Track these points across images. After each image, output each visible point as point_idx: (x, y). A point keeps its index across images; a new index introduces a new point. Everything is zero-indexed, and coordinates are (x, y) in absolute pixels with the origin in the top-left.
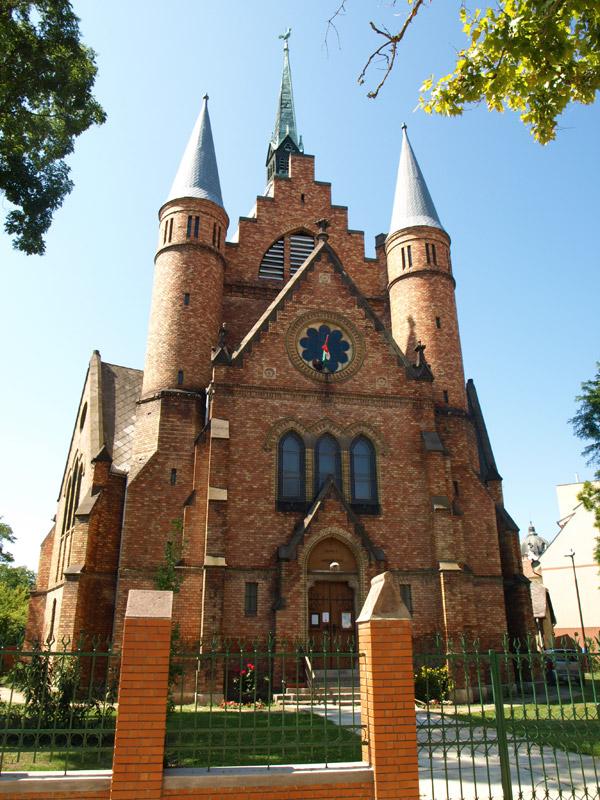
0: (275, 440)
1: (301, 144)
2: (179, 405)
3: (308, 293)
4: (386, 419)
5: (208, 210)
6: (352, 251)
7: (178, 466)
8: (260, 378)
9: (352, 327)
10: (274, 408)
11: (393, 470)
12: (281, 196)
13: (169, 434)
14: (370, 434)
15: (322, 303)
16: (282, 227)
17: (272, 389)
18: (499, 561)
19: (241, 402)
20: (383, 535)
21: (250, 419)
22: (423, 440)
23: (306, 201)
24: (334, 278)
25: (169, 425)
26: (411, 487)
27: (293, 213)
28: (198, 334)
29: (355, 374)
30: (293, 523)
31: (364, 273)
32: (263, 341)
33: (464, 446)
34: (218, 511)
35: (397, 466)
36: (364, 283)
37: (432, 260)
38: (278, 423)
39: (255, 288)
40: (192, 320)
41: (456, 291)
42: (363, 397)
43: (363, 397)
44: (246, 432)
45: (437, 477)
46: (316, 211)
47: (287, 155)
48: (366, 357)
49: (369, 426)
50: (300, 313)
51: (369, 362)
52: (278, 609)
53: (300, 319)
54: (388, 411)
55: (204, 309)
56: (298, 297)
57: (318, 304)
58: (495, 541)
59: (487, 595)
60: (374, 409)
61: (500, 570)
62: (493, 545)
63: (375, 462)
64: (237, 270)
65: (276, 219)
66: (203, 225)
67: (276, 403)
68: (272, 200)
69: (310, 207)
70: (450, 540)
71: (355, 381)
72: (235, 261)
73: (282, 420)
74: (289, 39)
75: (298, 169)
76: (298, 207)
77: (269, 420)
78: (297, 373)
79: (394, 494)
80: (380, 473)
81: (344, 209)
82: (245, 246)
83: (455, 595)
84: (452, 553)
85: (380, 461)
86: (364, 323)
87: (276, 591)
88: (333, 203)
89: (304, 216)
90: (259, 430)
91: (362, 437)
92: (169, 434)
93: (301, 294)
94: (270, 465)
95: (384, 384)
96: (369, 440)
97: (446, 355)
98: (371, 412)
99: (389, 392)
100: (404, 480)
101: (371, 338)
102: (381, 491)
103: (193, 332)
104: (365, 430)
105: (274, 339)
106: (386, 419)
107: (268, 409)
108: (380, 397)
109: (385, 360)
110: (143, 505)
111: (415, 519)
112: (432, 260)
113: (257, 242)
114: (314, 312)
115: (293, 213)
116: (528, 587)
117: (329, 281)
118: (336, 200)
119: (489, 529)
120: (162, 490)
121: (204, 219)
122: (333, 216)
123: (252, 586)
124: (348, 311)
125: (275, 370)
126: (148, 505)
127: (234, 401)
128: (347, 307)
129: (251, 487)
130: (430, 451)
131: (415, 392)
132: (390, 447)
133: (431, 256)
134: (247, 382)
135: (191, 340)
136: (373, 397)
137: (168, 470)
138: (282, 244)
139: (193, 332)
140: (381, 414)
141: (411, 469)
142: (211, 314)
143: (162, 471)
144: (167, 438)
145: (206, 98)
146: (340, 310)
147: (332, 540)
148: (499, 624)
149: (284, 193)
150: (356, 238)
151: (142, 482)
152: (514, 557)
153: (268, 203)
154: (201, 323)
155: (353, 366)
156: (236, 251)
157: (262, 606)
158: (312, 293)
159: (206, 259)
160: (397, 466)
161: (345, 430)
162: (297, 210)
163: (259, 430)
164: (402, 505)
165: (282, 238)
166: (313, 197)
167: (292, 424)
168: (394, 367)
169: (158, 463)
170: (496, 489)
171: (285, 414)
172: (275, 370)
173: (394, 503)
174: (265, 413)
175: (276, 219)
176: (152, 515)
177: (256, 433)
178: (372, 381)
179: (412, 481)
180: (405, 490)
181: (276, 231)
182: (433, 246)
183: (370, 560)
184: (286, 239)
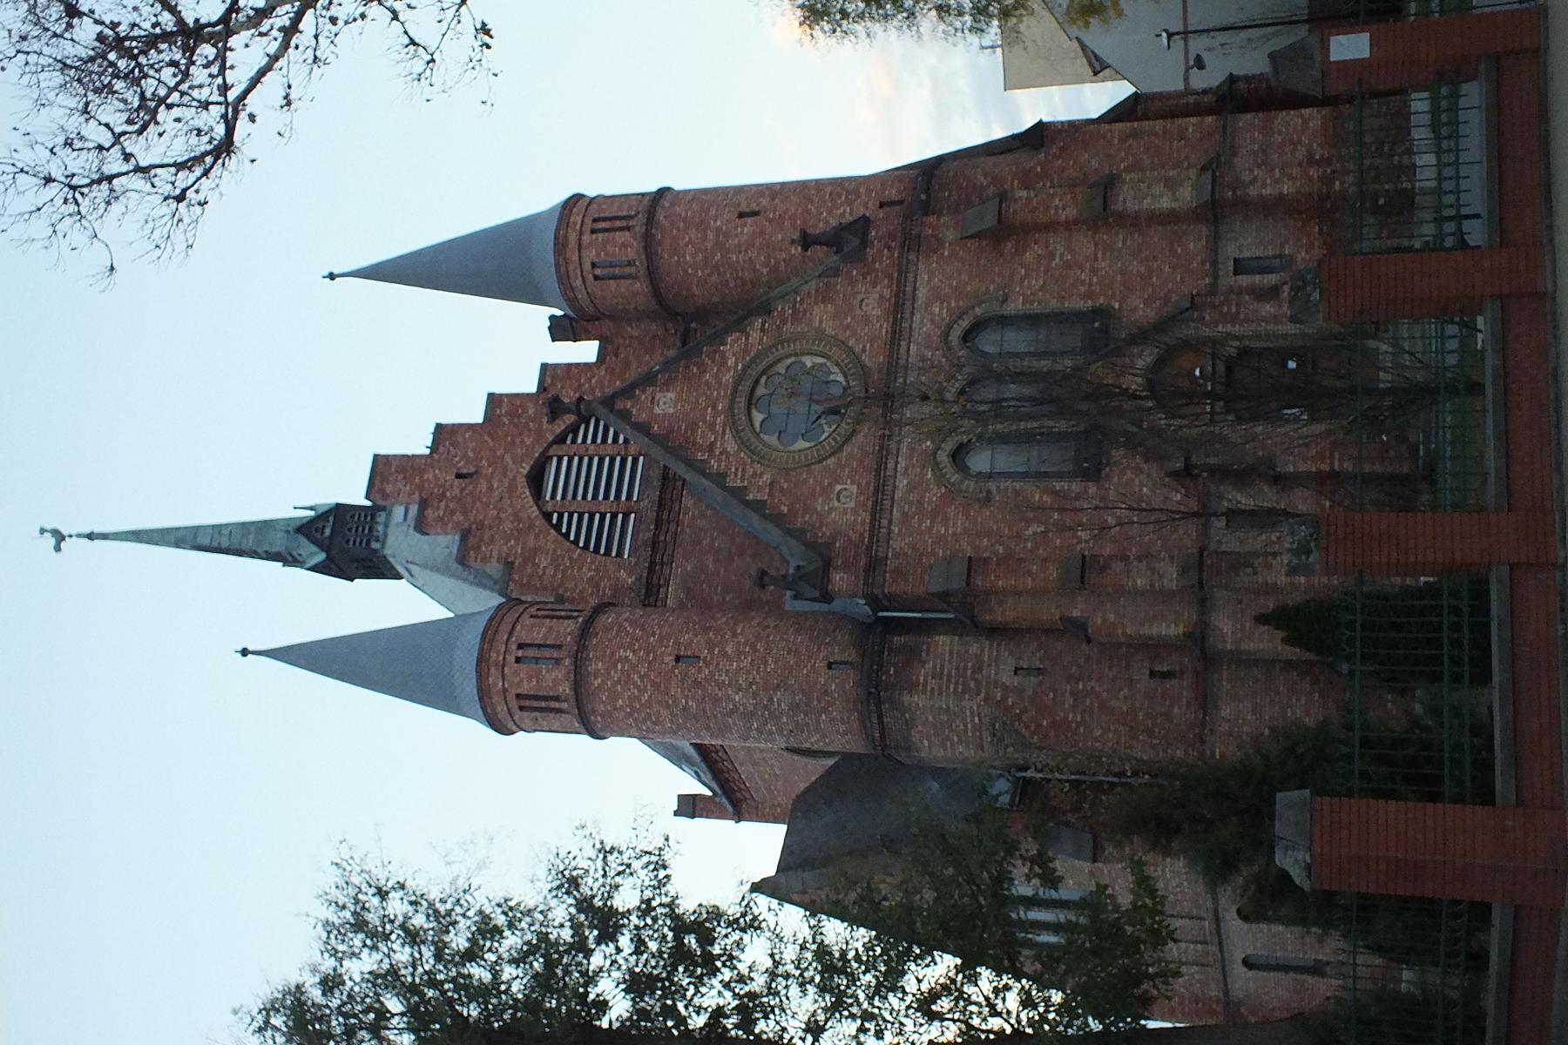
0: (970, 485)
1: (311, 508)
2: (895, 665)
3: (694, 431)
4: (937, 296)
5: (505, 627)
6: (580, 385)
7: (1011, 663)
8: (854, 511)
9: (761, 354)
10: (911, 488)
11: (1030, 286)
12: (459, 517)
13: (949, 681)
14: (965, 323)
15: (714, 407)
16: (523, 515)
17: (876, 490)
18: (1193, 120)
19: (896, 544)
21: (931, 527)
22: (977, 236)
23: (472, 470)
24: (666, 386)
25: (932, 683)
26: (1062, 256)
28: (758, 638)
29: (851, 349)
32: (785, 509)
33: (985, 175)
34: (1103, 569)
35: (1022, 280)
37: (623, 223)
38: (940, 478)
39: (652, 563)
40: (729, 650)
41: (677, 187)
42: (896, 336)
43: (896, 336)
44: (954, 534)
45: (1047, 208)
46: (493, 450)
47: (341, 542)
48: (820, 332)
49: (950, 327)
50: (731, 446)
51: (830, 328)
52: (1273, 467)
53: (743, 444)
54: (922, 294)
55: (709, 628)
57: (716, 414)
58: (1159, 125)
59: (1253, 140)
60: (917, 317)
61: (1210, 119)
62: (1165, 131)
63: (1016, 316)
65: (508, 526)
66: (538, 636)
67: (902, 483)
68: (465, 535)
69: (484, 463)
70: (1158, 188)
71: (864, 350)
73: (934, 474)
74: (65, 533)
75: (400, 485)
76: (483, 486)
77: (934, 495)
78: (847, 449)
79: (1074, 285)
80: (1036, 308)
81: (494, 400)
82: (561, 585)
83: (1255, 179)
84: (1181, 185)
85: (1014, 306)
86: (755, 336)
87: (1242, 476)
88: (479, 419)
90: (951, 511)
91: (966, 337)
92: (949, 681)
94: (1017, 493)
95: (872, 302)
97: (811, 201)
98: (924, 325)
99: (887, 293)
101: (784, 322)
103: (753, 646)
104: (957, 333)
105: (782, 490)
106: (937, 296)
107: (913, 497)
108: (899, 307)
110: (1083, 722)
112: (623, 223)
113: (555, 559)
114: (732, 421)
116: (1238, 78)
117: (671, 395)
118: (475, 414)
119: (1135, 135)
120: (1055, 692)
121: (522, 634)
122: (505, 420)
123: (1234, 516)
125: (839, 487)
126: (1083, 712)
127: (897, 555)
130: (999, 221)
131: (889, 248)
132: (987, 290)
133: (618, 224)
134: (862, 536)
135: (768, 650)
136: (895, 319)
137: (1016, 681)
138: (561, 516)
139: (753, 646)
140: (927, 305)
141: (1028, 256)
142: (716, 620)
143: (1019, 692)
144: (957, 683)
146: (728, 378)
148: (1305, 122)
149: (453, 512)
150: (553, 377)
151: (1039, 725)
152: (1184, 101)
153: (472, 541)
154: (734, 635)
155: (836, 353)
157: (1268, 497)
158: (693, 426)
159: (607, 629)
160: (1022, 280)
162: (491, 488)
163: (951, 511)
164: (1094, 271)
165: (547, 516)
166: (465, 456)
167: (943, 457)
168: (840, 284)
169: (1004, 698)
170: (1059, 132)
172: (839, 487)
173: (1090, 284)
174: (920, 502)
175: (508, 526)
176: (1101, 707)
178: (867, 320)
179: (1051, 255)
180: (1068, 266)
181: (532, 526)
182: (595, 220)
184: (549, 508)
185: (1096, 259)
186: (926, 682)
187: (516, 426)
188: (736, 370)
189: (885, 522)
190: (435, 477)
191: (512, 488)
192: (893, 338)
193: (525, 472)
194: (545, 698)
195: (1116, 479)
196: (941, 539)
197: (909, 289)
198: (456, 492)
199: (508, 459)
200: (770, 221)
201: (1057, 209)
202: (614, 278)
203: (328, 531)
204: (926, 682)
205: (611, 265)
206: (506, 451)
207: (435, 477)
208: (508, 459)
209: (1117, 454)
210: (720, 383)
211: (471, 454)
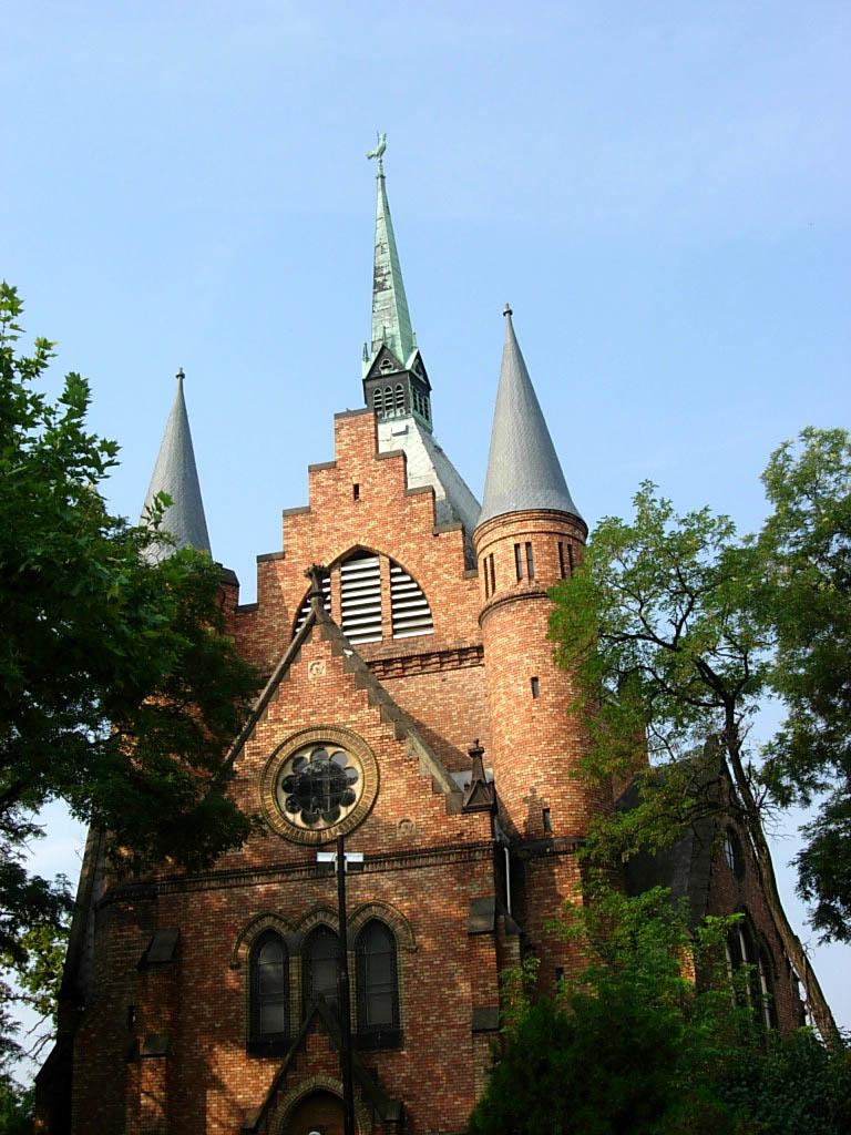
3: (291, 702)
15: (313, 714)
16: (325, 553)
20: (407, 1080)
21: (209, 923)
23: (361, 496)
27: (342, 524)
30: (272, 1073)
31: (463, 600)
36: (464, 619)
37: (524, 572)
54: (413, 874)
56: (277, 711)
57: (306, 716)
64: (258, 651)
71: (362, 834)
72: (254, 636)
76: (348, 511)
89: (359, 526)
93: (281, 705)
96: (386, 926)
100: (440, 985)
101: (390, 755)
102: (403, 1008)
109: (411, 788)
111: (457, 1048)
112: (524, 572)
115: (341, 524)
122: (407, 510)
124: (353, 717)
127: (186, 900)
128: (352, 710)
129: (213, 1026)
133: (524, 567)
145: (182, 376)
146: (339, 718)
147: (321, 1094)
149: (324, 493)
156: (254, 619)
160: (431, 963)
161: (295, 927)
164: (437, 1028)
166: (373, 485)
167: (267, 922)
171: (259, 907)
177: (217, 942)
180: (443, 1002)
183: (373, 1123)
185: (453, 1027)
186: (122, 937)
187: (402, 521)
188: (345, 724)
189: (213, 884)
190: (355, 467)
191: (346, 536)
192: (376, 857)
193: (361, 543)
194: (493, 580)
195: (248, 1072)
196: (199, 933)
197: (421, 862)
198: (343, 490)
199: (373, 524)
200: (529, 710)
201: (486, 985)
202: (562, 564)
203: (386, 372)
204: (122, 937)
205: (529, 560)
206: (379, 520)
207: (355, 467)
208: (373, 524)
209: (271, 1071)
210: (334, 713)
211: (376, 489)
